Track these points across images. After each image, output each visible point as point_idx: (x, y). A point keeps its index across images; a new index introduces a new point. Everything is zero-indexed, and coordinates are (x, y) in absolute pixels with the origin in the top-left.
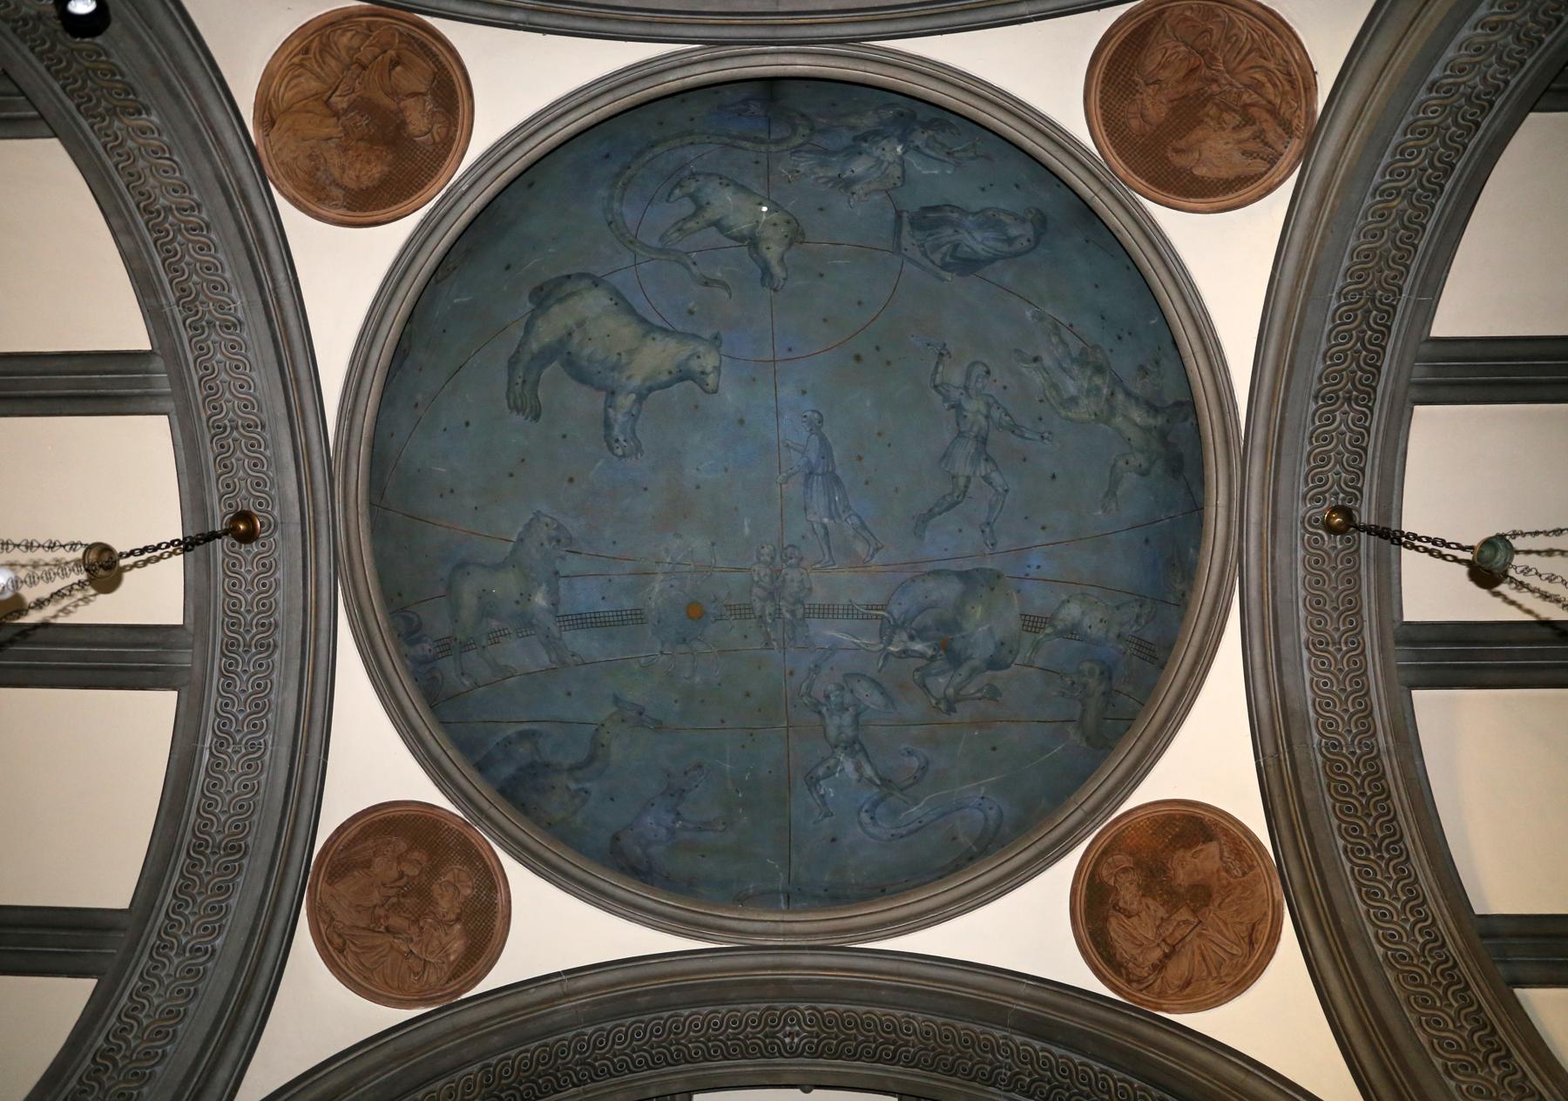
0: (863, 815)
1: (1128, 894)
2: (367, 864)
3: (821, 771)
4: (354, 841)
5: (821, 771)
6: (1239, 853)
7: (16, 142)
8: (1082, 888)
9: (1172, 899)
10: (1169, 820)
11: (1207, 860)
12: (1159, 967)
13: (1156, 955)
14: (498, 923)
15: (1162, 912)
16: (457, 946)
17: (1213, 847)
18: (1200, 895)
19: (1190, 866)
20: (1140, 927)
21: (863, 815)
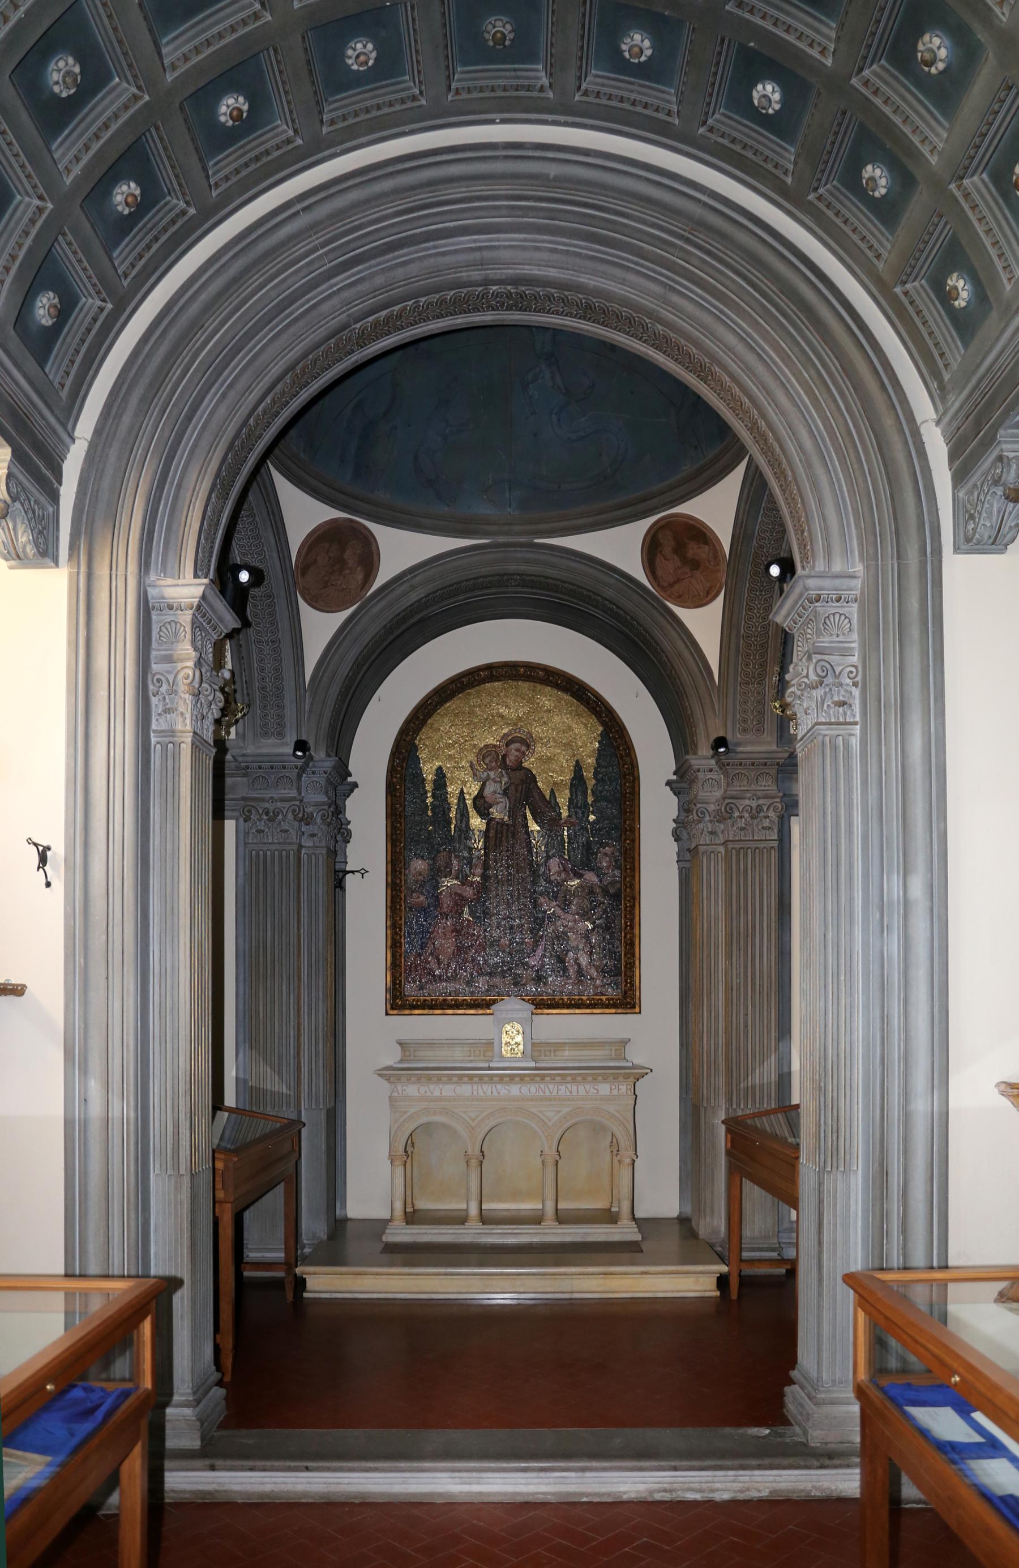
0: (553, 416)
1: (668, 550)
2: (315, 561)
3: (530, 376)
4: (307, 554)
5: (530, 376)
6: (716, 557)
7: (34, 362)
8: (649, 538)
9: (685, 560)
10: (693, 527)
11: (701, 552)
12: (671, 585)
13: (671, 580)
14: (375, 558)
15: (679, 564)
16: (360, 577)
17: (706, 548)
18: (695, 565)
19: (694, 550)
20: (669, 566)
21: (553, 416)
